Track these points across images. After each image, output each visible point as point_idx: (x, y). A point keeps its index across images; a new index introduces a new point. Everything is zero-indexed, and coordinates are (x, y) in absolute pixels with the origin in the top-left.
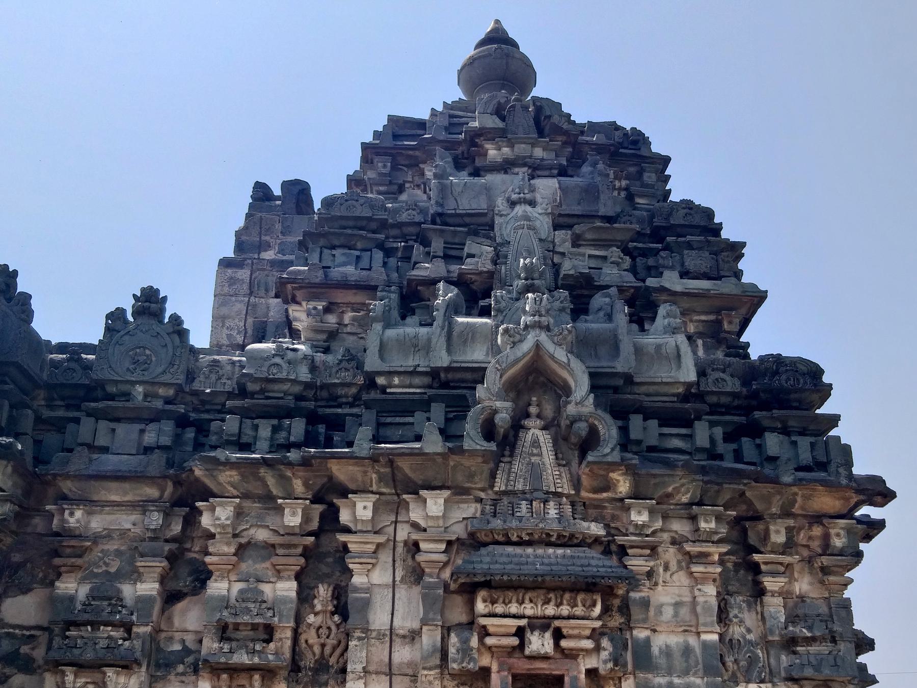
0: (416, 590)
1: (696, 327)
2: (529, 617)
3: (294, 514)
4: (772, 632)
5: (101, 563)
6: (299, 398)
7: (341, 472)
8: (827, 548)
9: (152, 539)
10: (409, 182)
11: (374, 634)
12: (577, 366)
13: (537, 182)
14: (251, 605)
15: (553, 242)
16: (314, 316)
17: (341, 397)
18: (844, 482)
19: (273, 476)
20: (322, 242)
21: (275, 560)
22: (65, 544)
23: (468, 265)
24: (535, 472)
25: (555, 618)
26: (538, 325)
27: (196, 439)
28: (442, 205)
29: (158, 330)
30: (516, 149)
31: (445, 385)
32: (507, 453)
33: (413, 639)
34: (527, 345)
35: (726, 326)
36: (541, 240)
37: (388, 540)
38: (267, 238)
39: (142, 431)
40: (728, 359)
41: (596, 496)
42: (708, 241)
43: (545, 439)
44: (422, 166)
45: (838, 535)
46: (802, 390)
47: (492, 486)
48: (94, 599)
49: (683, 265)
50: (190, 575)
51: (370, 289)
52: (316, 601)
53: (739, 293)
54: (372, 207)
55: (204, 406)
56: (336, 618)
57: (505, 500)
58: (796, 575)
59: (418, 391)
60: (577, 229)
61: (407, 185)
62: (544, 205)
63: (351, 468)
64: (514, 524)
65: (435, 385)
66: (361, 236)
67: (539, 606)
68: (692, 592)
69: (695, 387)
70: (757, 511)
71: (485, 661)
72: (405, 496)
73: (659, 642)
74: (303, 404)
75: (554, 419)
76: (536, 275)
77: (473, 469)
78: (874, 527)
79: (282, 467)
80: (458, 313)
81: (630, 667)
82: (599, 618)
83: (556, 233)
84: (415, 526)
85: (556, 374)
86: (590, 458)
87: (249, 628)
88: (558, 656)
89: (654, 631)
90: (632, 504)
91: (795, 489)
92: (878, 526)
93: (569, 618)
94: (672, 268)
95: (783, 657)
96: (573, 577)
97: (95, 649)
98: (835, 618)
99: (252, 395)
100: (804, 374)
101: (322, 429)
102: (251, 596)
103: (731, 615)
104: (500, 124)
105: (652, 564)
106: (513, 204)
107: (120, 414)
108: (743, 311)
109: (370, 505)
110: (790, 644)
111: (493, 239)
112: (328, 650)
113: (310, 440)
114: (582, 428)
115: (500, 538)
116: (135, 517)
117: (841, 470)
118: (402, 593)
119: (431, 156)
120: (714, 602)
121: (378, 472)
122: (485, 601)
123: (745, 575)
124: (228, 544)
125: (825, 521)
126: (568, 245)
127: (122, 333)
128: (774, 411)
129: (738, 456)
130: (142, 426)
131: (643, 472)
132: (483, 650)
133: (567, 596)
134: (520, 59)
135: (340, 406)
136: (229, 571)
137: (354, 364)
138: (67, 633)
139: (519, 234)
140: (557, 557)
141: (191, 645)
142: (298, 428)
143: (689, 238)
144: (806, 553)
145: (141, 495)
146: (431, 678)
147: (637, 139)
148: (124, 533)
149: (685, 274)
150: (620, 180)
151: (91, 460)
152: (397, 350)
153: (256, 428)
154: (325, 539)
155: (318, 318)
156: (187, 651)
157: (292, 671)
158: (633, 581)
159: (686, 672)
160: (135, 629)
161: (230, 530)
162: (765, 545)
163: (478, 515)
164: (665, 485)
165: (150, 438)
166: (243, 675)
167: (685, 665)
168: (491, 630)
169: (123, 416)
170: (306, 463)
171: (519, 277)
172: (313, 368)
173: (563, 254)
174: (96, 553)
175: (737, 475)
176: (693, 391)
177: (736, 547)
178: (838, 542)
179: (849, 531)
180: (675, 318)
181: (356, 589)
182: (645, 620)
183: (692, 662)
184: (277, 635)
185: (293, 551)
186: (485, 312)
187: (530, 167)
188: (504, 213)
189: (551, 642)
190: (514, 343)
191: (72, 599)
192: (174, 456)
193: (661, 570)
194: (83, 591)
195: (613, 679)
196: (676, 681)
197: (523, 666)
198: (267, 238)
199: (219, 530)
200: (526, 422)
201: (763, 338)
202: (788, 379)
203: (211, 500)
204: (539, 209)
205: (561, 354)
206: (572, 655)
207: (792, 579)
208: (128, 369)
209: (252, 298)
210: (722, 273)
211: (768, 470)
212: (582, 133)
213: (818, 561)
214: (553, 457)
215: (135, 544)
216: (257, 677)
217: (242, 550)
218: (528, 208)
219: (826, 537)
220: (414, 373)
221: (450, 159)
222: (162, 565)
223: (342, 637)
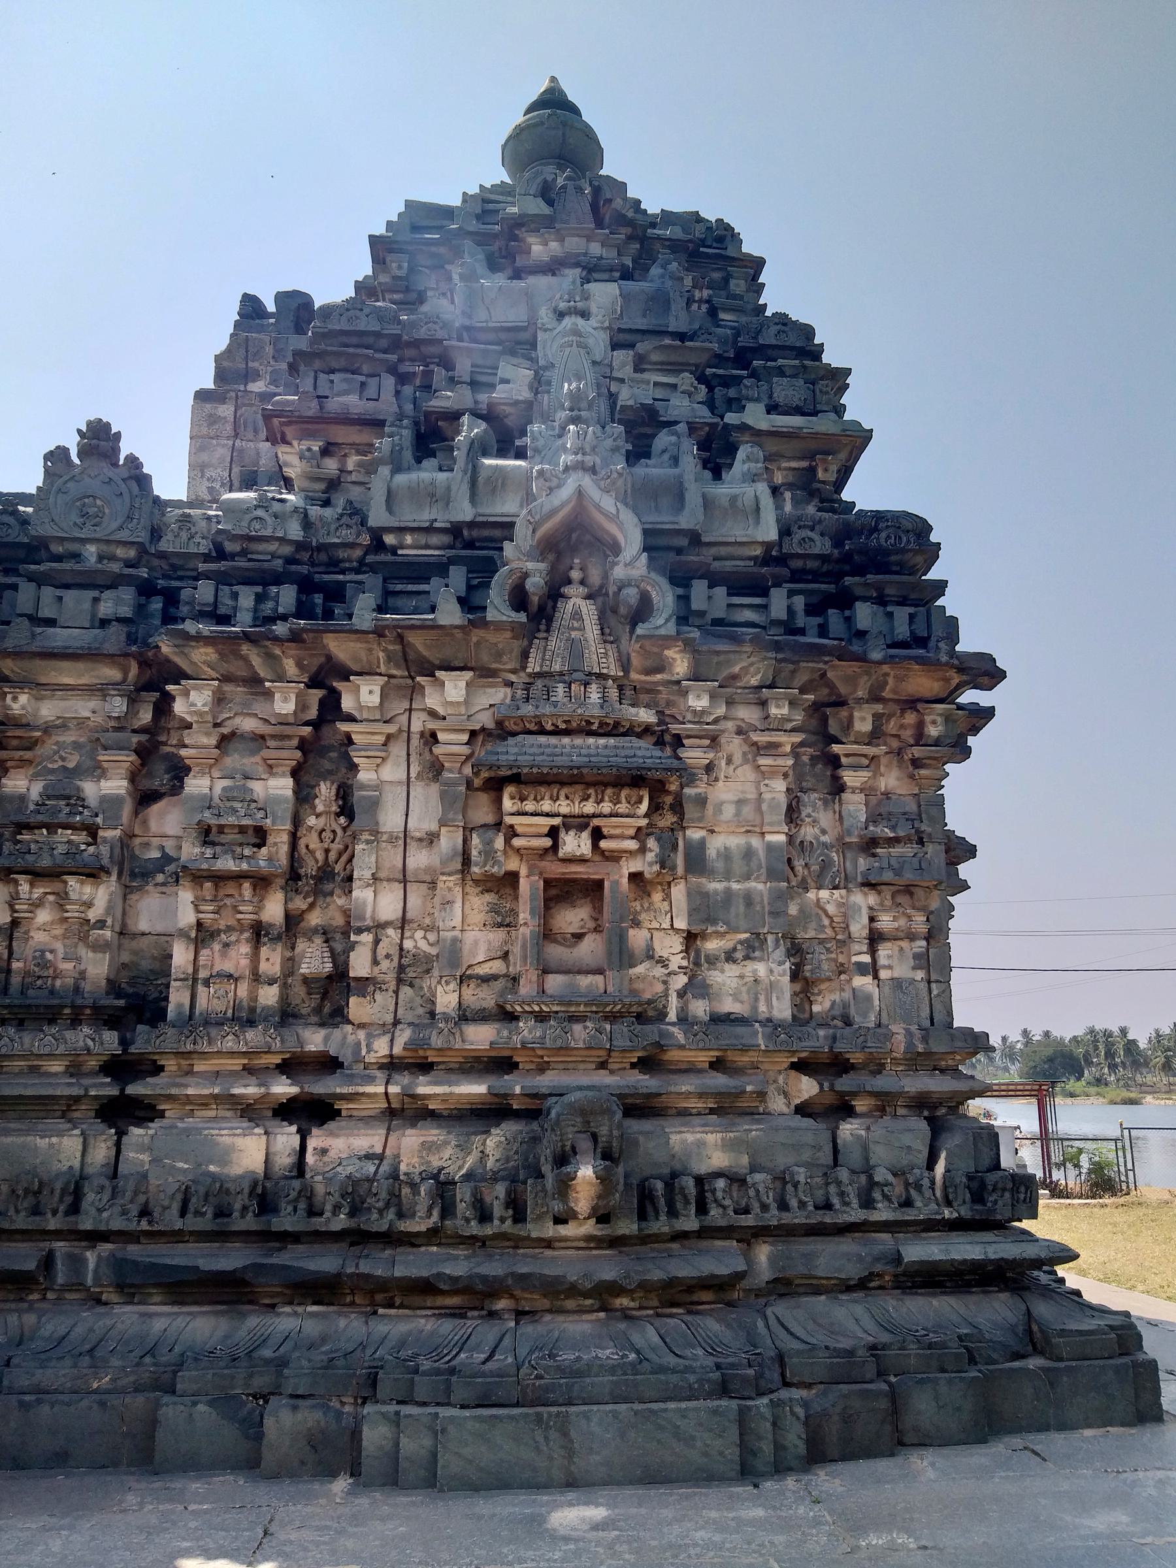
0: (435, 788)
1: (784, 477)
2: (565, 816)
3: (286, 700)
4: (849, 833)
5: (56, 758)
6: (290, 561)
7: (341, 648)
8: (920, 737)
9: (117, 729)
10: (433, 289)
11: (385, 837)
12: (628, 517)
13: (592, 287)
14: (237, 805)
15: (610, 366)
16: (309, 460)
17: (342, 561)
18: (944, 658)
19: (258, 655)
20: (317, 364)
21: (266, 753)
22: (9, 734)
23: (500, 393)
24: (576, 650)
25: (594, 816)
26: (580, 466)
27: (165, 610)
28: (470, 317)
29: (110, 474)
30: (566, 244)
31: (470, 545)
32: (543, 627)
33: (432, 842)
34: (567, 491)
35: (820, 474)
36: (594, 363)
37: (400, 731)
38: (255, 365)
39: (96, 600)
40: (819, 514)
41: (648, 678)
42: (804, 367)
43: (589, 610)
44: (447, 266)
45: (934, 722)
46: (903, 551)
47: (524, 668)
48: (49, 799)
49: (771, 397)
50: (167, 772)
51: (376, 424)
52: (317, 801)
53: (838, 432)
54: (380, 319)
55: (175, 571)
56: (342, 820)
57: (539, 683)
58: (882, 769)
59: (437, 552)
60: (641, 347)
61: (429, 294)
62: (600, 317)
63: (352, 644)
64: (547, 709)
65: (458, 545)
66: (367, 356)
67: (577, 803)
68: (758, 788)
69: (776, 548)
70: (839, 695)
71: (513, 864)
72: (418, 679)
73: (715, 844)
74: (293, 568)
75: (601, 587)
76: (584, 405)
77: (500, 646)
78: (982, 716)
79: (268, 643)
80: (485, 454)
81: (680, 870)
82: (646, 815)
83: (615, 353)
84: (433, 714)
85: (604, 530)
86: (640, 630)
87: (236, 831)
88: (597, 858)
89: (712, 832)
90: (689, 686)
91: (886, 668)
92: (988, 714)
93: (611, 815)
94: (758, 400)
95: (861, 860)
96: (614, 770)
97: (52, 855)
98: (923, 816)
99: (232, 556)
100: (908, 531)
101: (318, 599)
102: (239, 795)
103: (803, 814)
104: (546, 210)
105: (711, 755)
106: (561, 315)
107: (68, 579)
108: (843, 456)
109: (377, 690)
110: (870, 845)
111: (534, 360)
112: (332, 856)
113: (303, 610)
114: (631, 595)
115: (532, 727)
116: (94, 703)
117: (942, 645)
118: (418, 790)
119: (458, 253)
120: (783, 800)
121: (385, 650)
122: (512, 798)
123: (823, 767)
124: (207, 734)
125: (920, 706)
126: (629, 369)
127: (65, 478)
128: (869, 576)
129: (823, 631)
130: (96, 593)
131: (704, 648)
132: (510, 852)
133: (609, 791)
134: (581, 130)
135: (343, 572)
136: (211, 767)
137: (357, 519)
138: (19, 837)
139: (567, 353)
140: (598, 748)
141: (171, 852)
142: (287, 596)
143: (780, 362)
144: (895, 744)
145: (98, 677)
146: (451, 884)
147: (724, 234)
148: (81, 722)
149: (772, 409)
150: (701, 289)
151: (33, 635)
152: (410, 501)
153: (235, 596)
154: (326, 730)
155: (314, 462)
156: (166, 859)
157: (290, 879)
158: (687, 775)
159: (747, 877)
160: (101, 833)
161: (209, 718)
162: (847, 735)
163: (508, 701)
164: (729, 663)
165: (106, 608)
166: (231, 883)
167: (746, 868)
168: (519, 830)
169: (73, 582)
170: (295, 637)
171: (562, 407)
172: (307, 524)
173: (622, 381)
174: (48, 748)
175: (816, 651)
176: (774, 553)
177: (813, 738)
178: (933, 731)
179: (948, 719)
180: (757, 462)
181: (363, 787)
182: (701, 819)
183: (754, 865)
184: (271, 840)
185: (287, 743)
186: (520, 454)
187: (584, 268)
188: (549, 327)
189: (589, 842)
190: (551, 489)
191: (23, 798)
192: (137, 632)
193: (723, 763)
194: (36, 790)
195: (661, 884)
196: (735, 886)
197: (556, 870)
198: (255, 365)
199: (195, 718)
200: (566, 590)
201: (866, 490)
202: (888, 537)
203: (183, 682)
204: (593, 322)
205: (609, 503)
206: (613, 857)
207: (877, 774)
208: (75, 524)
209: (238, 441)
210: (819, 407)
211: (856, 648)
212: (653, 225)
213: (909, 752)
214: (599, 632)
215: (96, 735)
216: (247, 885)
217: (225, 741)
218: (580, 321)
219: (920, 726)
220: (429, 530)
221: (481, 256)
222: (130, 759)
223: (348, 840)
